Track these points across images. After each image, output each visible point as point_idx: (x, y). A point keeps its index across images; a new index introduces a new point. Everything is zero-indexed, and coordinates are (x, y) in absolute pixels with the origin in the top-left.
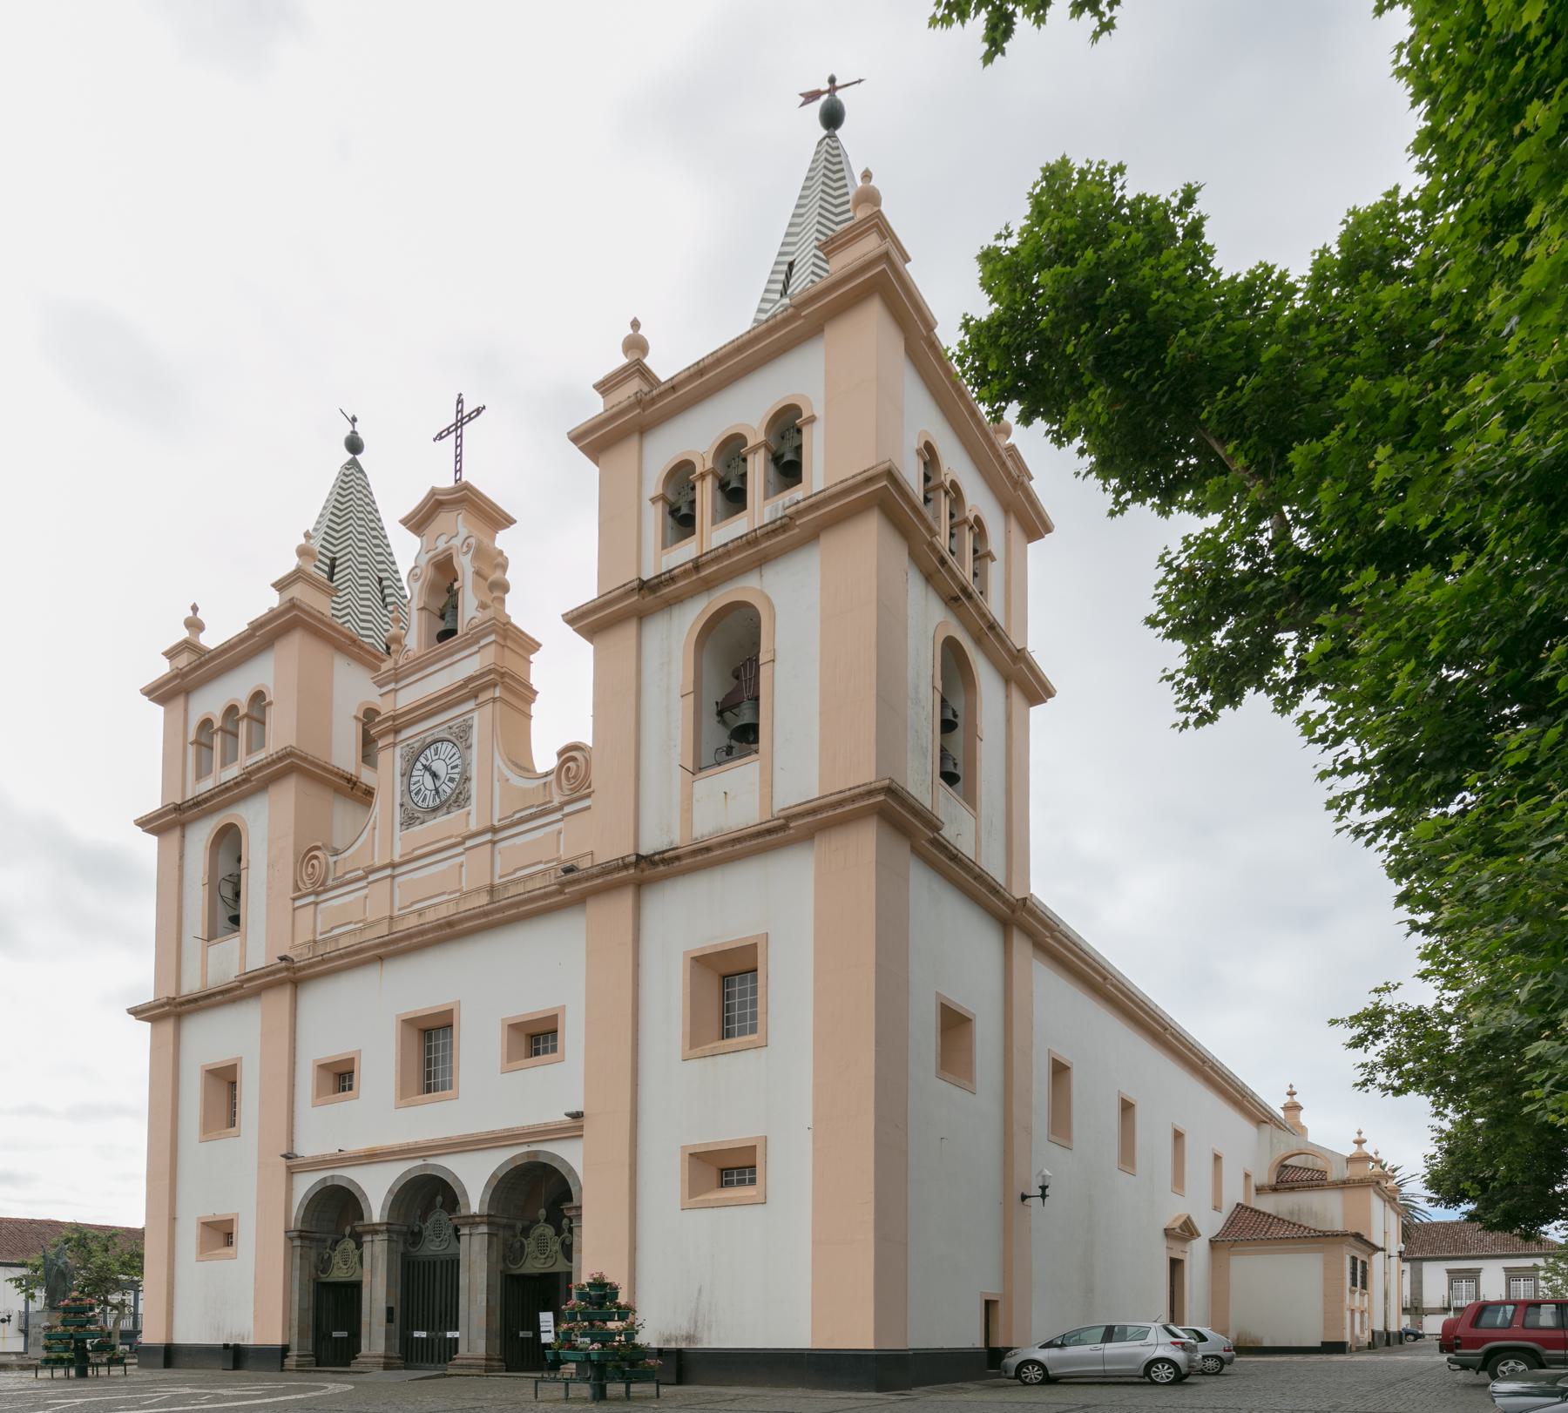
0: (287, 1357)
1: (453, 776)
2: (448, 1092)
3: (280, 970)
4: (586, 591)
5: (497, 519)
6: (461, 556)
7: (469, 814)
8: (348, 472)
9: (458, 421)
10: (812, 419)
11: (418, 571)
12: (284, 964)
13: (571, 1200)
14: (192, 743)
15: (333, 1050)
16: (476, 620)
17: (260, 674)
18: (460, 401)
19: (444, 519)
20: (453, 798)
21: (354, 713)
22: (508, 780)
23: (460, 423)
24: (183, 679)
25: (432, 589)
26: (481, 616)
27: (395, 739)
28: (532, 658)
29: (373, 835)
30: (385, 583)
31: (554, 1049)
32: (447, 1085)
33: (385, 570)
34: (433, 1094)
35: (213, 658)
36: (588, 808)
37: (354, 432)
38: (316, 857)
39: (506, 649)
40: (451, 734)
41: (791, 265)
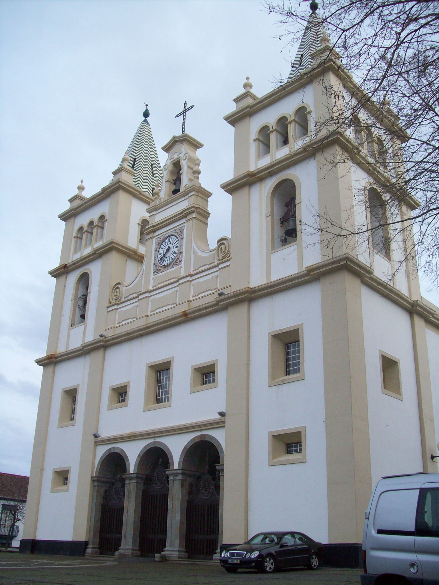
0: (87, 548)
1: (175, 251)
2: (166, 403)
3: (99, 342)
4: (229, 176)
5: (196, 145)
6: (183, 161)
7: (181, 268)
8: (143, 125)
9: (184, 111)
10: (310, 112)
11: (166, 167)
12: (101, 339)
13: (219, 463)
14: (74, 237)
15: (118, 382)
16: (187, 186)
17: (103, 208)
18: (185, 104)
19: (177, 147)
20: (175, 261)
21: (138, 222)
22: (197, 253)
23: (185, 111)
24: (251, 109)
25: (172, 173)
26: (190, 184)
27: (153, 235)
28: (209, 199)
29: (142, 277)
30: (153, 166)
31: (213, 381)
32: (166, 400)
33: (154, 161)
34: (160, 404)
35: (261, 102)
36: (229, 265)
37: (147, 110)
38: (118, 288)
39: (198, 197)
40: (176, 233)
41: (302, 55)
